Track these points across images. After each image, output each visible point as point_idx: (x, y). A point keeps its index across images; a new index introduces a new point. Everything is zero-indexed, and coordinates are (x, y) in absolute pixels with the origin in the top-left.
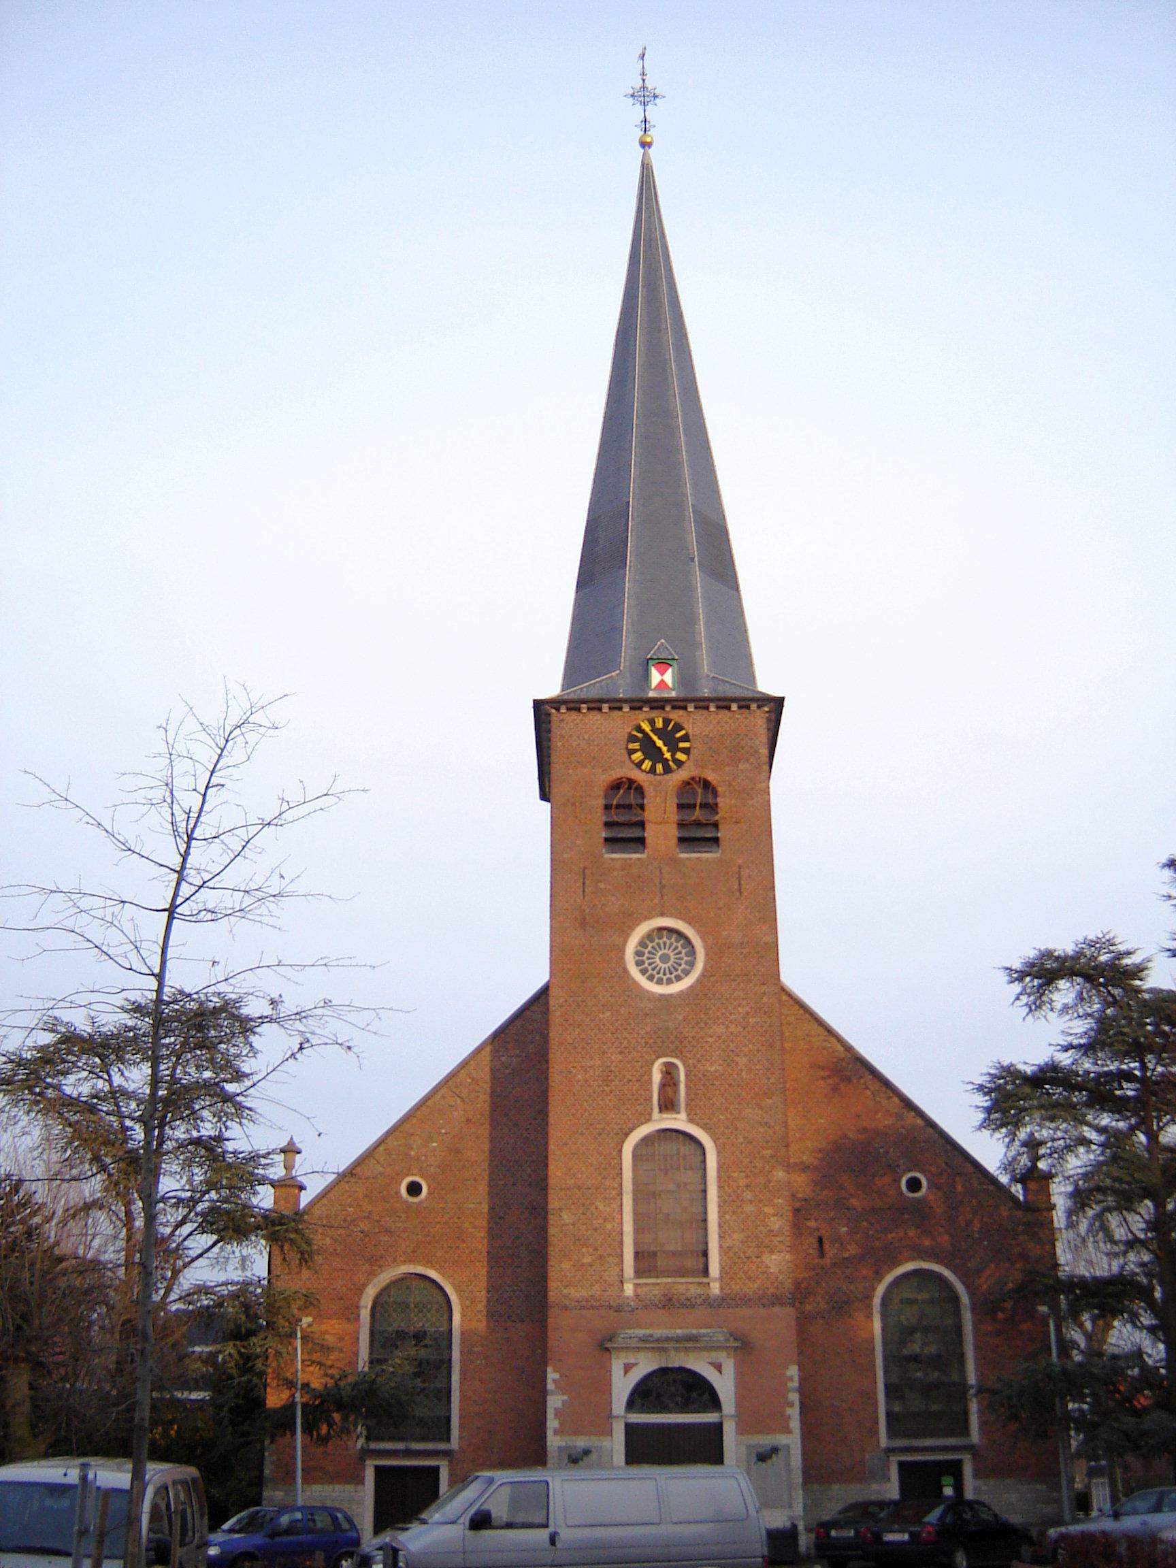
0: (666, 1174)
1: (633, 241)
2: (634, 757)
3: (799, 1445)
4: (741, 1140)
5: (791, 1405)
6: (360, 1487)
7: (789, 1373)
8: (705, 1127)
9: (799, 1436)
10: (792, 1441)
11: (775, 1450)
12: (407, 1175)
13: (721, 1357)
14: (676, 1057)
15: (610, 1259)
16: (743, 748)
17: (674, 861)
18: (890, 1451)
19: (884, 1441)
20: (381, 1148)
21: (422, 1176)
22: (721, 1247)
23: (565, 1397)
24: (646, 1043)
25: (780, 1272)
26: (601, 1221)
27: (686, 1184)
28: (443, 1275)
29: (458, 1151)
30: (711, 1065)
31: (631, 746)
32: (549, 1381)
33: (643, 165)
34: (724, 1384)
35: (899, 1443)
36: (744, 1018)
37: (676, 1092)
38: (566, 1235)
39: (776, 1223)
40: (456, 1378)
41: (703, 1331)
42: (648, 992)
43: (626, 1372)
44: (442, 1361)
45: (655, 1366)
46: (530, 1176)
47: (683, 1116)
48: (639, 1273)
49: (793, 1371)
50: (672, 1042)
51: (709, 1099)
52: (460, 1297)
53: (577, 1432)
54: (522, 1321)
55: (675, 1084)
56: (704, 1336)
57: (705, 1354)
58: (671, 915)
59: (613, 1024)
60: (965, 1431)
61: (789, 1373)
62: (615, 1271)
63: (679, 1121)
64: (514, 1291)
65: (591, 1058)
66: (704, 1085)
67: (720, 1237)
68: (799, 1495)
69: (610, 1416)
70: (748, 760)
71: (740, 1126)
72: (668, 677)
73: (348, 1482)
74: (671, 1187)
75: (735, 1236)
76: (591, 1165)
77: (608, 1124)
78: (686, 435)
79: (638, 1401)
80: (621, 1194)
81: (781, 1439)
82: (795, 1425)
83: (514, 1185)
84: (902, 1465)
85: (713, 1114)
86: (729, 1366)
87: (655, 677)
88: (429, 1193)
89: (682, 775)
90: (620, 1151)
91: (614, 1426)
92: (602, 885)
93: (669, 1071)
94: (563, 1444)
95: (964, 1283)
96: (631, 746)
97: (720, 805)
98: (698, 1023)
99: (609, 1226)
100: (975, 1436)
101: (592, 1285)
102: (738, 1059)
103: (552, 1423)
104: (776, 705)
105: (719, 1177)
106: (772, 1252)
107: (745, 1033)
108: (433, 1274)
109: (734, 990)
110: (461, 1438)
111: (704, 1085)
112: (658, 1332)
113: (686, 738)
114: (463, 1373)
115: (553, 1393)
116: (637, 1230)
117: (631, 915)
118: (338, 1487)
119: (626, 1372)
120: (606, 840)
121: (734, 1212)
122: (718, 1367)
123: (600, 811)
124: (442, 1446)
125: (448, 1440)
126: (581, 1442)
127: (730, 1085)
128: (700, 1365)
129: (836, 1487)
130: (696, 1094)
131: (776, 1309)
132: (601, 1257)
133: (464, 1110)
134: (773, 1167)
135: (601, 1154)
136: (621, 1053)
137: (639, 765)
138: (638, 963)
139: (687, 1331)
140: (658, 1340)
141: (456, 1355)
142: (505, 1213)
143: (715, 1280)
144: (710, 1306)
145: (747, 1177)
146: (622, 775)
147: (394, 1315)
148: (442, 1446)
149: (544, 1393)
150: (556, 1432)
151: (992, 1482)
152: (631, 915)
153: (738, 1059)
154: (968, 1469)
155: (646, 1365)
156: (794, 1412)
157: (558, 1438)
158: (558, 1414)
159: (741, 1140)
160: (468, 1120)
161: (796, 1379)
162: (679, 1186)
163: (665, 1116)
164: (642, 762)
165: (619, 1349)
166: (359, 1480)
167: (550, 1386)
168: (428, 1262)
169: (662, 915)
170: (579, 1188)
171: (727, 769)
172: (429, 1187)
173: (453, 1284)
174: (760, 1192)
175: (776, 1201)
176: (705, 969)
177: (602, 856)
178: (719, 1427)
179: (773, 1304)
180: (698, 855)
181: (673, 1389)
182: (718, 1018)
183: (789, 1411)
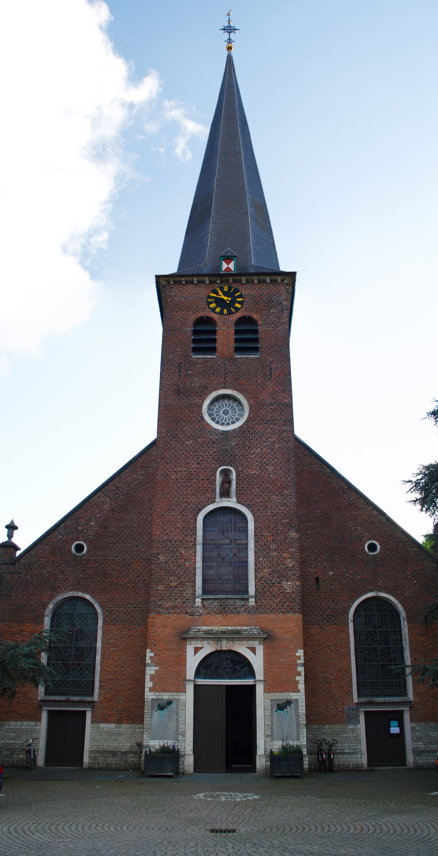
0: (223, 534)
1: (222, 86)
2: (211, 306)
3: (304, 700)
4: (269, 514)
5: (299, 674)
6: (38, 723)
7: (297, 654)
8: (248, 506)
9: (304, 694)
10: (300, 696)
11: (289, 702)
12: (76, 541)
13: (256, 644)
14: (231, 466)
15: (188, 584)
16: (273, 301)
17: (232, 360)
18: (359, 704)
19: (356, 700)
20: (62, 526)
21: (84, 541)
22: (256, 577)
23: (157, 668)
24: (213, 458)
25: (293, 592)
26: (183, 561)
27: (235, 540)
28: (93, 598)
29: (105, 527)
30: (252, 471)
31: (209, 300)
32: (148, 658)
33: (228, 56)
34: (257, 661)
35: (364, 700)
36: (272, 444)
37: (230, 486)
38: (161, 569)
39: (290, 563)
40: (98, 658)
41: (245, 628)
42: (215, 429)
43: (195, 653)
44: (91, 648)
45: (214, 650)
46: (147, 541)
47: (234, 499)
48: (205, 592)
49: (300, 653)
50: (229, 458)
51: (251, 490)
52: (103, 610)
53: (164, 690)
54: (139, 625)
55: (229, 482)
56: (245, 630)
57: (245, 642)
58: (230, 388)
59: (194, 448)
60: (404, 693)
61: (297, 654)
62: (190, 591)
63: (231, 502)
64: (135, 607)
65: (180, 467)
66: (248, 482)
67: (255, 571)
68: (304, 731)
69: (185, 680)
70: (276, 308)
71: (269, 506)
72: (232, 266)
73: (32, 720)
74: (227, 541)
75: (265, 570)
76: (178, 528)
77: (189, 504)
78: (245, 161)
79: (203, 671)
80: (195, 545)
81: (293, 696)
82: (301, 686)
83: (137, 546)
84: (366, 713)
85: (253, 498)
86: (260, 649)
87: (225, 266)
88: (88, 551)
89: (239, 315)
90: (196, 520)
91: (187, 686)
92: (190, 372)
93: (226, 473)
94: (155, 697)
95: (403, 605)
96: (209, 300)
97: (260, 330)
98: (244, 447)
99: (187, 564)
100: (411, 696)
101: (176, 599)
102: (268, 467)
103: (148, 684)
104: (293, 275)
105: (256, 535)
106: (287, 580)
107: (273, 453)
108: (88, 597)
109: (266, 429)
110: (100, 694)
111: (248, 482)
112: (216, 628)
113: (241, 296)
114: (103, 656)
115: (150, 665)
116: (204, 568)
117: (207, 388)
118: (26, 723)
119: (195, 653)
120: (193, 348)
121: (264, 556)
122: (253, 650)
123: (190, 334)
124: (88, 699)
125: (93, 695)
126: (166, 696)
127: (263, 482)
128: (242, 649)
129: (327, 726)
130: (242, 487)
131: (290, 615)
132: (182, 583)
133: (111, 504)
134: (289, 530)
135: (184, 521)
136: (198, 464)
137: (213, 310)
138: (210, 415)
139: (235, 628)
140: (216, 633)
141: (99, 644)
142: (131, 562)
143: (252, 597)
144: (249, 613)
145: (273, 535)
146: (204, 315)
147: (65, 621)
148: (88, 699)
149: (145, 665)
150: (151, 690)
151: (422, 724)
152: (207, 388)
153: (268, 467)
154: (407, 717)
155: (208, 648)
156: (301, 679)
157: (152, 693)
158: (151, 679)
159: (269, 514)
160: (113, 510)
161: (302, 658)
162: (231, 541)
163: (223, 499)
164: (215, 308)
165: (192, 638)
166: (39, 719)
167: (148, 661)
168: (85, 590)
169: (225, 388)
170: (170, 541)
171: (264, 312)
172: (88, 547)
173: (99, 603)
174: (281, 544)
175: (290, 550)
176: (249, 417)
177: (191, 357)
178: (252, 688)
179: (288, 612)
180: (246, 356)
181: (225, 664)
182: (257, 444)
183: (298, 678)
